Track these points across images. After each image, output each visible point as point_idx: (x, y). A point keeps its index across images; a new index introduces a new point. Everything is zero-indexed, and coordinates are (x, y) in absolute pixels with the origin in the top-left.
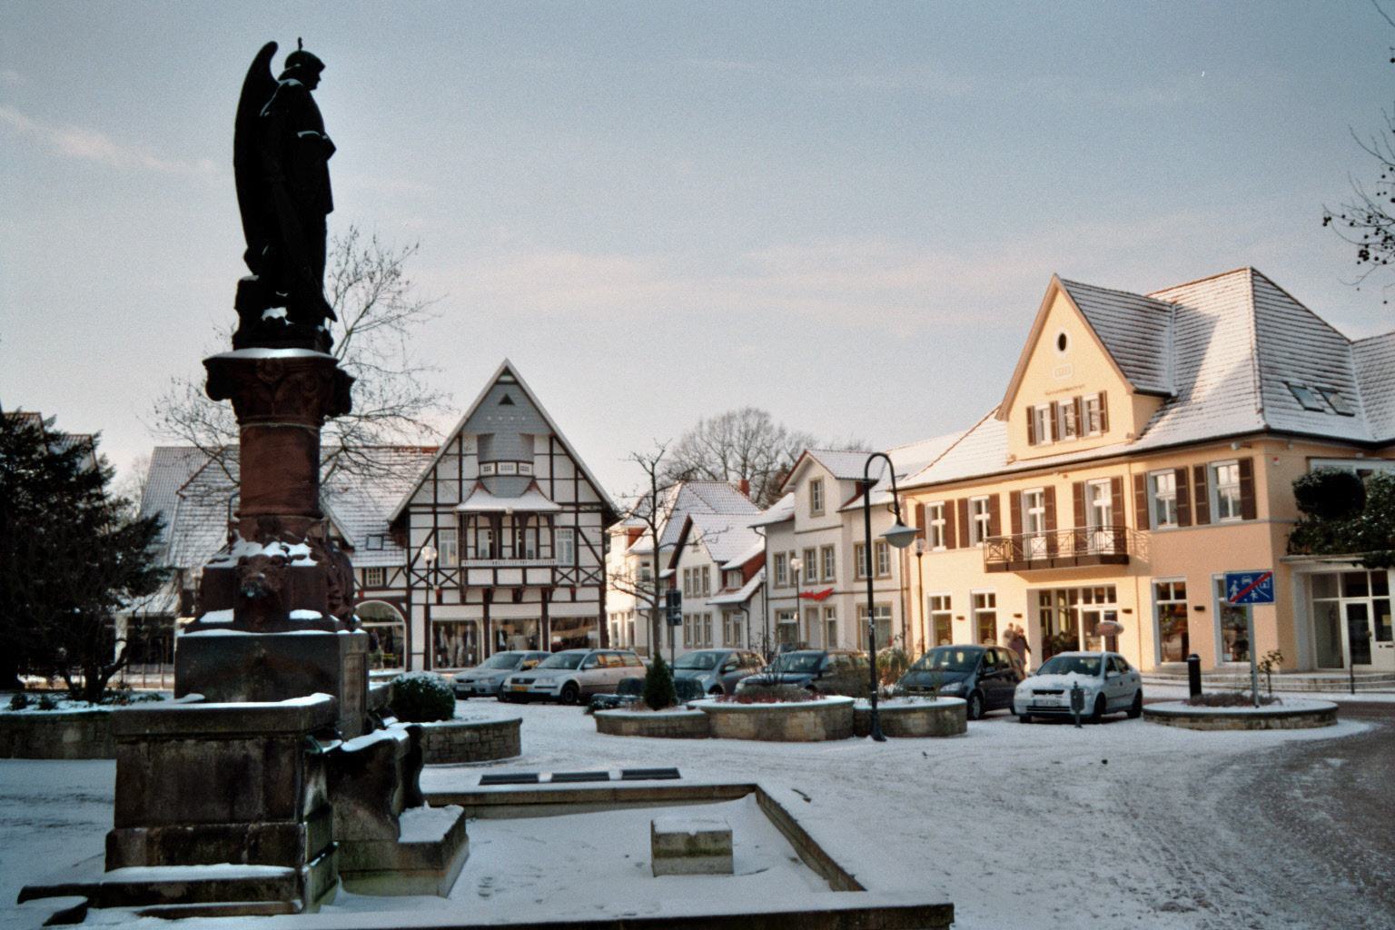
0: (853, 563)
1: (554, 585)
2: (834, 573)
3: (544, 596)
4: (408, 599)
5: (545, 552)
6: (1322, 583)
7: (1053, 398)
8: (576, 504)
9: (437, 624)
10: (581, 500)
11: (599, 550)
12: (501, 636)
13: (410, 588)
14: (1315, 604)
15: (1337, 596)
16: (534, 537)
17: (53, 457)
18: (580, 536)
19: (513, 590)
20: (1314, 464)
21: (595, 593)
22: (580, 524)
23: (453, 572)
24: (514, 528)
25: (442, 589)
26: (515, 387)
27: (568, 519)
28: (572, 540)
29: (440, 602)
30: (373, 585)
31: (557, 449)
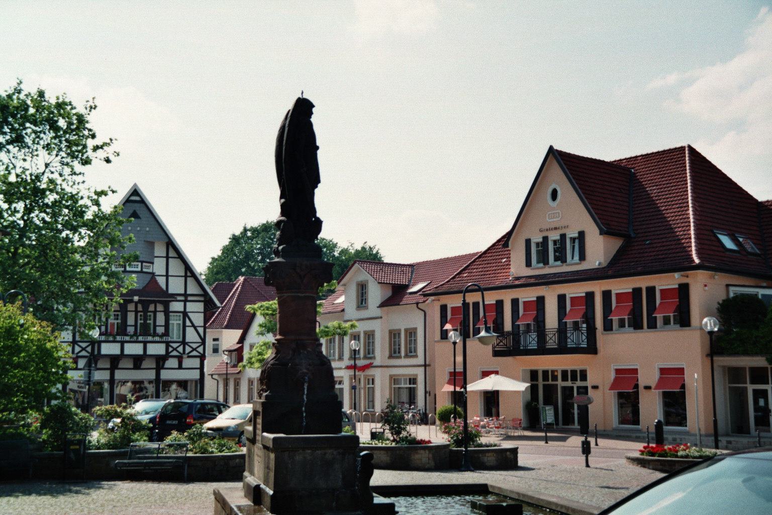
0: (387, 345)
1: (166, 356)
2: (373, 352)
3: (158, 363)
6: (735, 374)
7: (545, 234)
8: (185, 295)
10: (188, 292)
11: (201, 330)
14: (730, 387)
15: (746, 383)
17: (68, 290)
18: (187, 320)
19: (111, 358)
20: (733, 291)
21: (196, 363)
22: (188, 310)
23: (87, 344)
24: (136, 312)
25: (78, 357)
26: (142, 205)
28: (181, 322)
31: (172, 253)
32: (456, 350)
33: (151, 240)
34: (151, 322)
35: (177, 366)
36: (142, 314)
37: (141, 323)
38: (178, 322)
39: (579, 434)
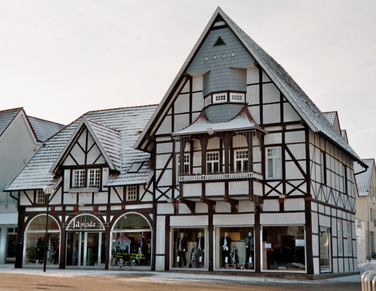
4: (154, 210)
5: (257, 168)
8: (282, 124)
9: (177, 231)
10: (285, 120)
12: (225, 242)
13: (155, 202)
16: (117, 155)
18: (286, 153)
21: (301, 204)
22: (286, 142)
27: (277, 138)
29: (176, 213)
30: (131, 200)
32: (318, 222)
33: (245, 67)
38: (216, 161)
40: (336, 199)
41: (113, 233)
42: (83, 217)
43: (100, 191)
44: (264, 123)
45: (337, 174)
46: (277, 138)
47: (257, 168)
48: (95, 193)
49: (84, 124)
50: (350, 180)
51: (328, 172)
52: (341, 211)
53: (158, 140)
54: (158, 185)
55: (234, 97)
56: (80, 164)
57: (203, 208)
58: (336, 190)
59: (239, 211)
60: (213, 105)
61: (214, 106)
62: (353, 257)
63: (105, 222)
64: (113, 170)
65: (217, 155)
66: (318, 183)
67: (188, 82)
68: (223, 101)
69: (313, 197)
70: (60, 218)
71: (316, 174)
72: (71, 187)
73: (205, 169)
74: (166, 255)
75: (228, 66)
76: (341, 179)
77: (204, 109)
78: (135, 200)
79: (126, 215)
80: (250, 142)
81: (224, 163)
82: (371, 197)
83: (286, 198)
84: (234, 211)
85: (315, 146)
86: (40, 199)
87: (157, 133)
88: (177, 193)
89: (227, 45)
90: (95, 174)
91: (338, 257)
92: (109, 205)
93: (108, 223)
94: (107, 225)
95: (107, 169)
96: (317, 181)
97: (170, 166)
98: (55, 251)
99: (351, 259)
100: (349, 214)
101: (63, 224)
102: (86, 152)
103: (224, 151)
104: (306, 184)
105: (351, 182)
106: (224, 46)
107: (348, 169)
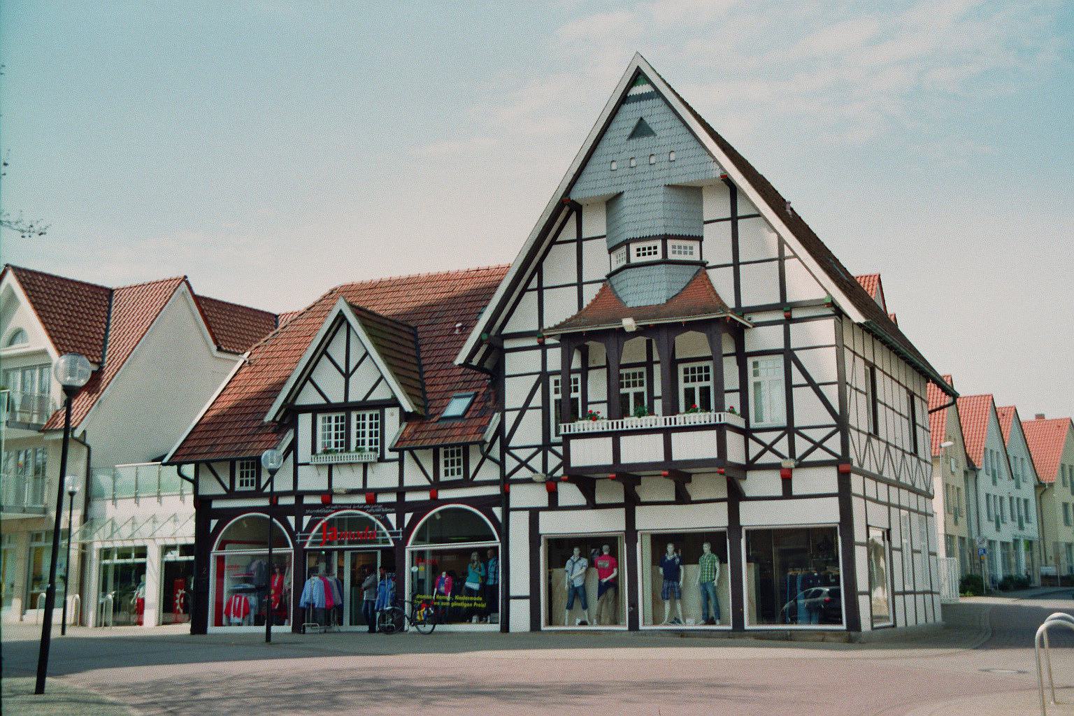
4: (503, 500)
8: (784, 305)
13: (505, 482)
18: (794, 368)
21: (828, 480)
29: (553, 505)
30: (450, 478)
34: (578, 395)
35: (780, 493)
36: (559, 378)
37: (556, 401)
39: (1001, 593)
40: (897, 466)
41: (412, 552)
42: (340, 520)
43: (382, 459)
44: (744, 304)
45: (897, 412)
46: (770, 337)
47: (732, 400)
48: (369, 466)
49: (341, 311)
50: (921, 424)
51: (880, 407)
52: (907, 492)
53: (508, 344)
54: (512, 444)
55: (677, 250)
56: (333, 400)
57: (610, 492)
58: (896, 447)
59: (693, 499)
60: (629, 266)
61: (643, 268)
62: (931, 593)
63: (393, 529)
64: (408, 412)
65: (641, 375)
66: (864, 433)
67: (574, 216)
68: (653, 258)
69: (855, 464)
70: (292, 520)
71: (859, 416)
72: (314, 451)
73: (618, 407)
74: (534, 597)
75: (661, 182)
76: (905, 422)
77: (609, 276)
78: (461, 477)
79: (440, 512)
80: (715, 344)
81: (658, 391)
82: (947, 458)
83: (797, 467)
84: (682, 498)
85: (854, 353)
86: (245, 479)
87: (505, 331)
88: (553, 461)
89: (658, 136)
90: (367, 422)
91: (904, 593)
92: (401, 491)
93: (401, 530)
94: (398, 534)
95: (396, 411)
96: (860, 428)
97: (537, 400)
98: (491, 586)
99: (928, 597)
100: (921, 499)
101: (299, 534)
102: (347, 375)
103: (657, 369)
104: (838, 434)
105: (923, 428)
106: (652, 137)
107: (917, 400)
